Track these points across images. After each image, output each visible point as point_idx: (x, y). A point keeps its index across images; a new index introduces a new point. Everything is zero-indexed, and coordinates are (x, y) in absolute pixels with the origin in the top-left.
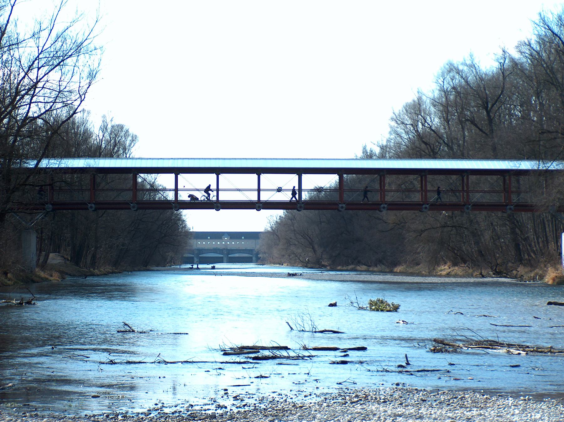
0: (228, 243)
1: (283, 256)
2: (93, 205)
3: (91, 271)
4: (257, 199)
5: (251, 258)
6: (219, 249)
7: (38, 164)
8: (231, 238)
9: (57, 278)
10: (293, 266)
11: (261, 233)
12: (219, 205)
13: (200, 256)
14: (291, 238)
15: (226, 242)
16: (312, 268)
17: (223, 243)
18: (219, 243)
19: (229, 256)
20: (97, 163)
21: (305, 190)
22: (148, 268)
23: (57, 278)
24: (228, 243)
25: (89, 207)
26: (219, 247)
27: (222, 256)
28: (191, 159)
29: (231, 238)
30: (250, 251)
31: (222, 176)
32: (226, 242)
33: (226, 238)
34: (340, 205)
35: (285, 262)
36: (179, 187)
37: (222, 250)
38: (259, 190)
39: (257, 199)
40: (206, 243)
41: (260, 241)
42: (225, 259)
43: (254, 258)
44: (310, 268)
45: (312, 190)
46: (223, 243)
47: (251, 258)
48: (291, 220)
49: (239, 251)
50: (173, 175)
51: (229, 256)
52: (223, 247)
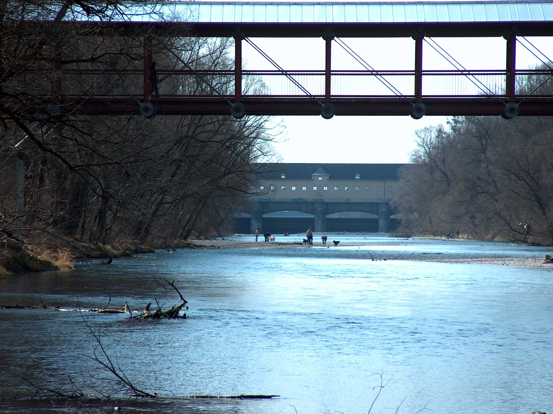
0: (326, 188)
1: (458, 217)
2: (150, 105)
3: (99, 249)
4: (323, 93)
5: (376, 221)
6: (306, 203)
7: (62, 14)
8: (331, 178)
9: (68, 263)
10: (483, 240)
11: (402, 168)
12: (422, 106)
13: (265, 216)
14: (479, 179)
15: (320, 187)
16: (539, 245)
17: (315, 188)
18: (304, 188)
19: (327, 216)
20: (195, 13)
21: (524, 72)
22: (189, 241)
23: (68, 263)
24: (326, 188)
25: (141, 109)
26: (304, 197)
27: (313, 216)
28: (295, 4)
29: (331, 178)
30: (373, 206)
31: (428, 43)
32: (320, 187)
33: (320, 179)
34: (508, 106)
35: (464, 232)
36: (425, 66)
37: (313, 203)
38: (328, 73)
39: (413, 93)
40: (299, 189)
41: (400, 183)
42: (319, 223)
43: (382, 223)
44: (533, 244)
45: (537, 72)
46: (315, 188)
47: (376, 221)
48: (480, 138)
49: (350, 206)
50: (501, 43)
51: (327, 216)
52: (313, 197)
